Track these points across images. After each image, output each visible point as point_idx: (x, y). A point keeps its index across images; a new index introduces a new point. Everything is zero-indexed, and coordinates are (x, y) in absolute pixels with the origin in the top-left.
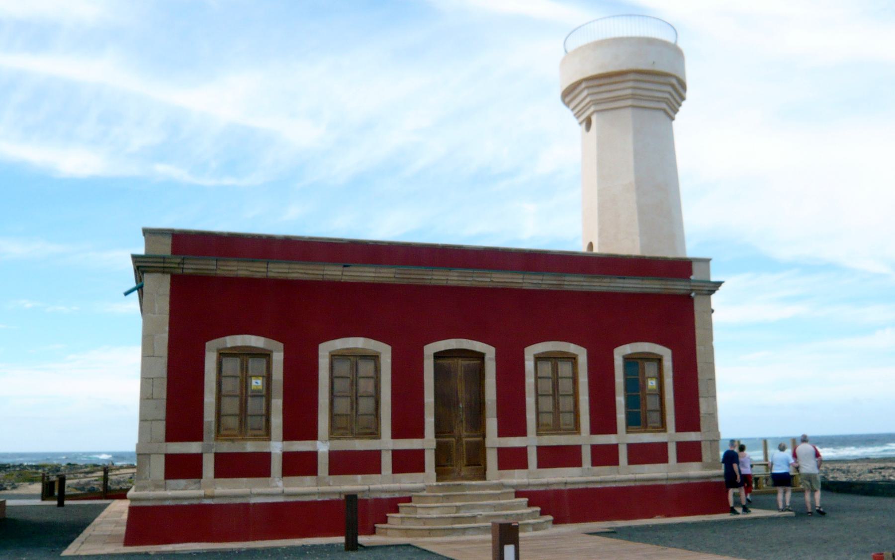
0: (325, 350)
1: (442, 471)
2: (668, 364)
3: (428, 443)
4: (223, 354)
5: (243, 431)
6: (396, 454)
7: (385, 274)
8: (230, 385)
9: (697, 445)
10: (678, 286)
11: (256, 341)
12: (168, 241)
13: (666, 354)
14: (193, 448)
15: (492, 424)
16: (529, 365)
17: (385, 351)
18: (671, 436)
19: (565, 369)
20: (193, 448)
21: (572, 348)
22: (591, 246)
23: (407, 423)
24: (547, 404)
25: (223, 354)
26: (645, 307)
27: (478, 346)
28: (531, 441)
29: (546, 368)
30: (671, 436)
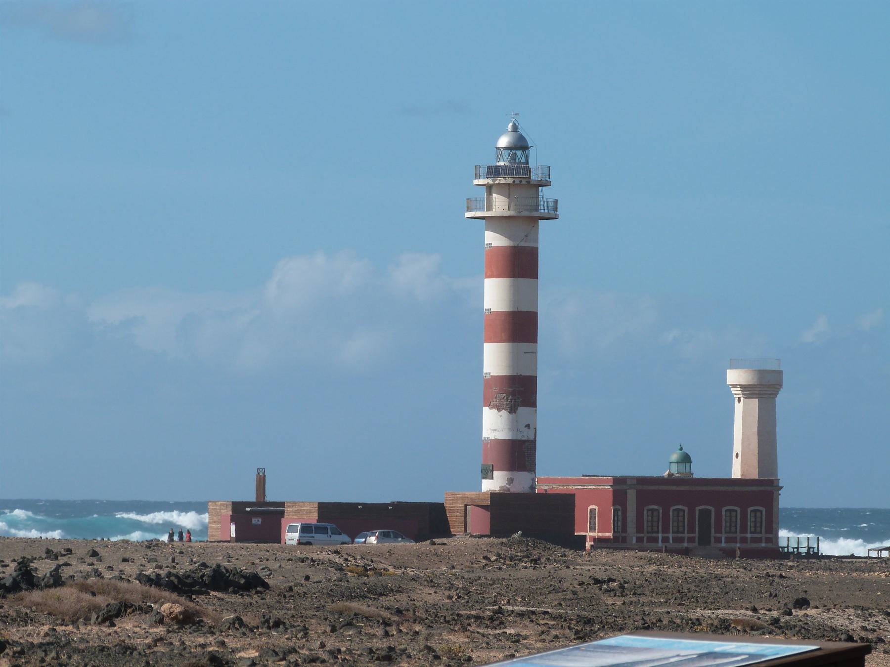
0: (724, 509)
1: (699, 544)
2: (764, 513)
3: (696, 535)
4: (648, 510)
5: (653, 532)
6: (688, 538)
7: (704, 488)
8: (681, 524)
9: (771, 538)
10: (769, 488)
11: (656, 507)
12: (532, 438)
13: (764, 510)
14: (642, 535)
15: (713, 530)
16: (724, 513)
17: (686, 509)
18: (763, 535)
19: (733, 514)
20: (642, 535)
21: (736, 508)
22: (686, 459)
23: (691, 530)
24: (675, 524)
25: (648, 510)
26: (757, 498)
27: (736, 508)
28: (749, 535)
29: (728, 513)
30: (763, 535)
